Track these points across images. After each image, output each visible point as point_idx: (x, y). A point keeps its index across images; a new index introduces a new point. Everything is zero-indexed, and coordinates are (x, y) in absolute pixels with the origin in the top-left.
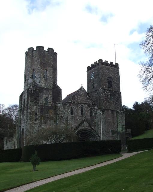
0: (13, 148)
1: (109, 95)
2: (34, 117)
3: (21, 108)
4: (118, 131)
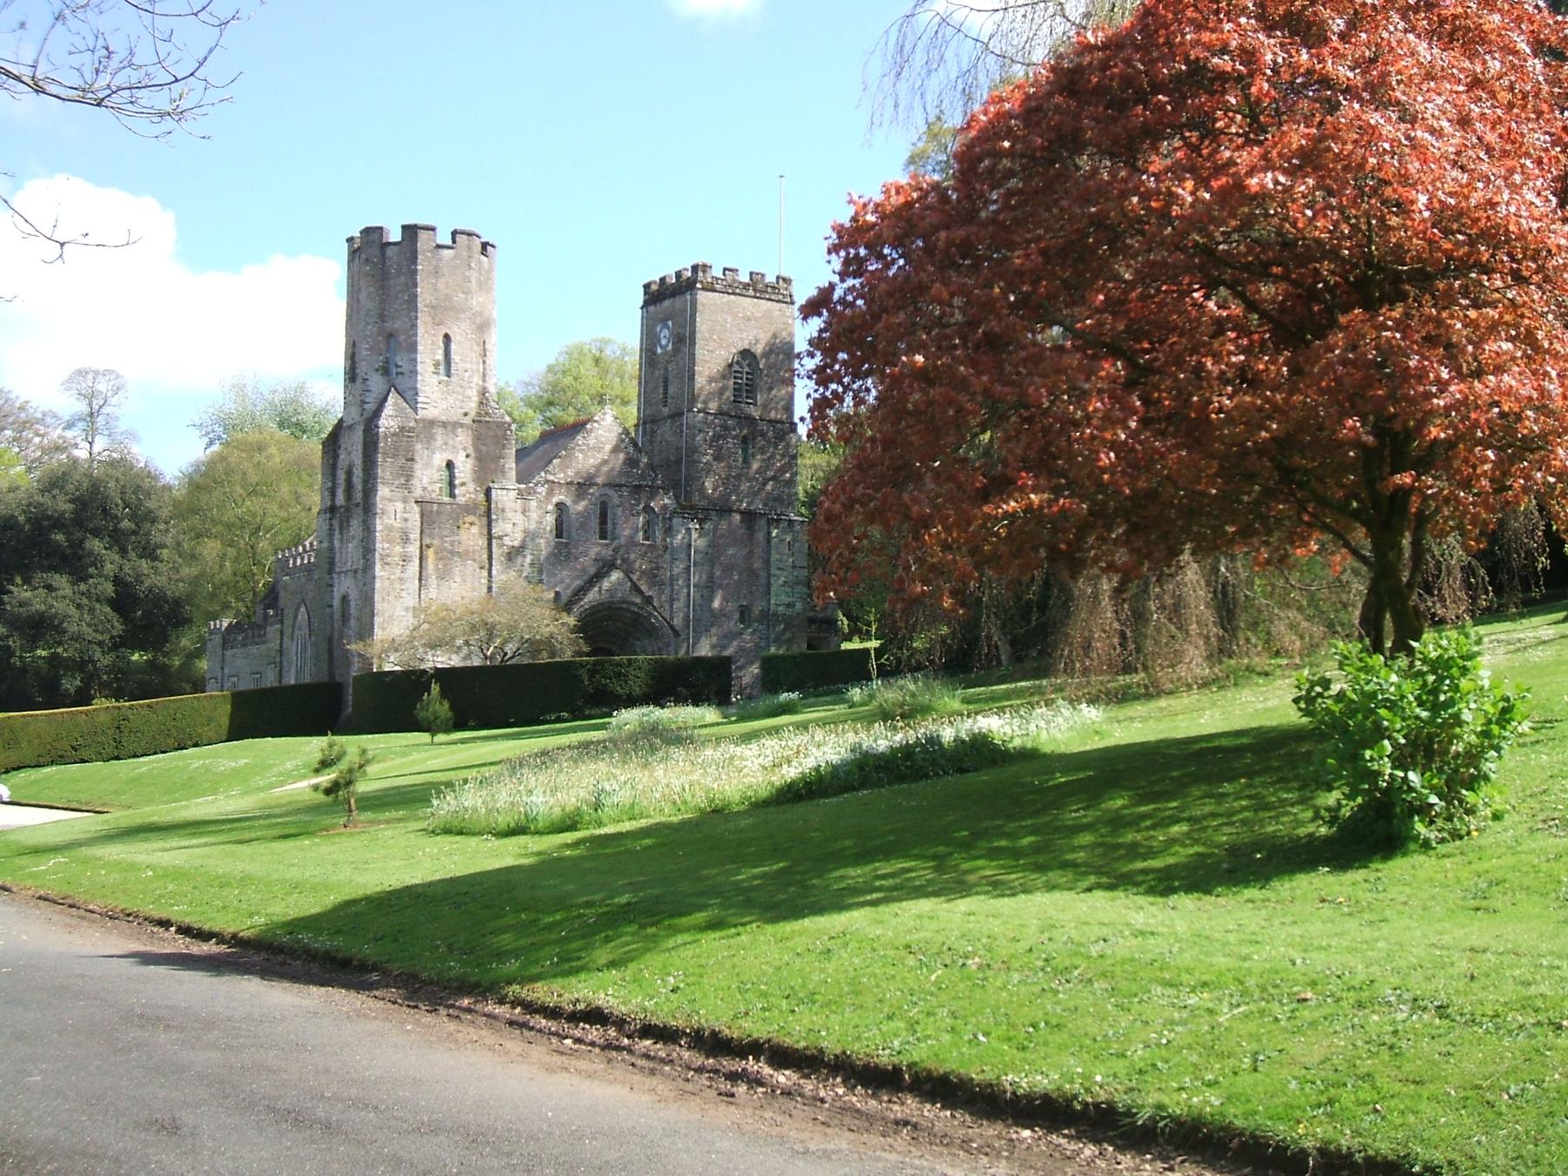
0: (270, 680)
1: (734, 438)
2: (398, 549)
3: (333, 500)
4: (772, 607)
